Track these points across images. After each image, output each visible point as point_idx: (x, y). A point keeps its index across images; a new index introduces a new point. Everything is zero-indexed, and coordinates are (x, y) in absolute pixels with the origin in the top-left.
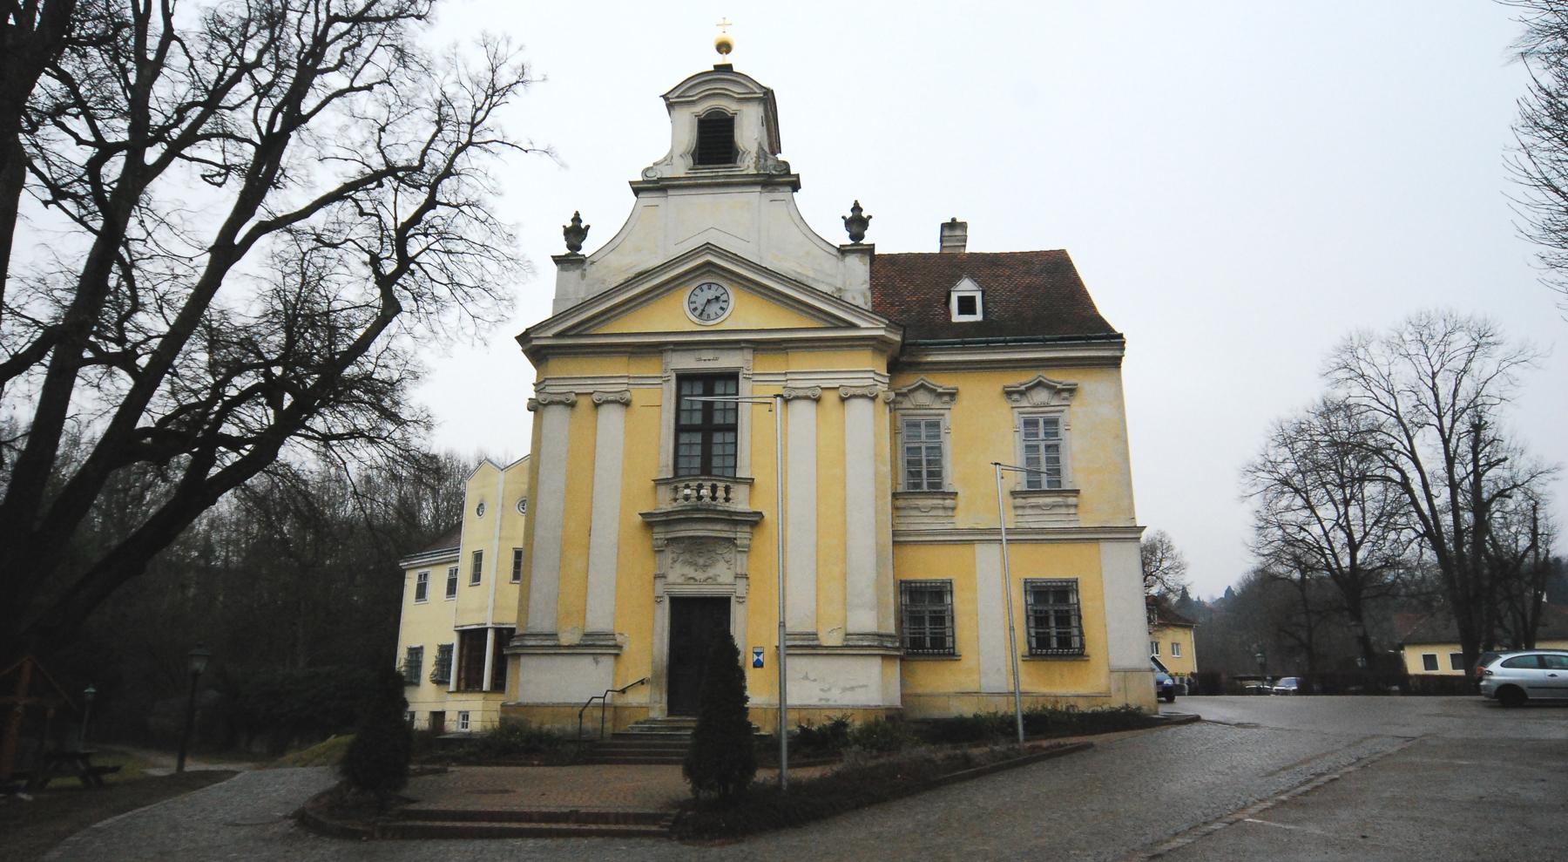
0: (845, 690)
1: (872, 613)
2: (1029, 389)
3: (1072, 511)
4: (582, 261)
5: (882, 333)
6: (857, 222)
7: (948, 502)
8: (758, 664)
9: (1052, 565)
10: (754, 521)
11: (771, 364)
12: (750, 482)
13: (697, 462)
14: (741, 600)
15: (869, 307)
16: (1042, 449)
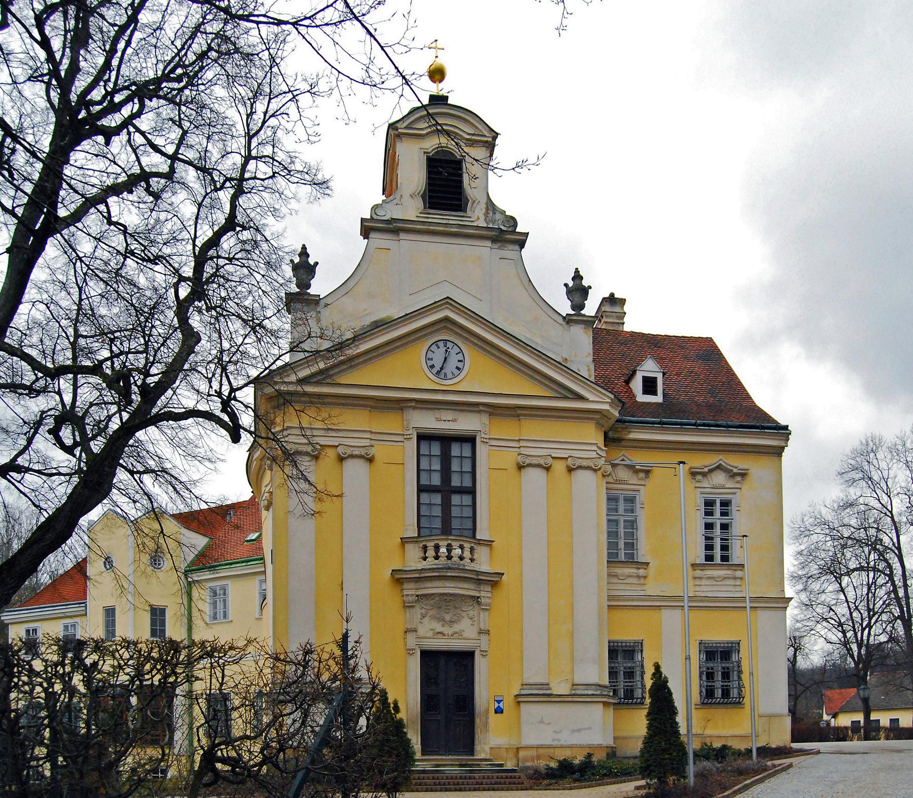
0: (573, 731)
1: (596, 672)
2: (711, 471)
3: (738, 582)
4: (316, 301)
5: (607, 407)
6: (578, 291)
7: (642, 572)
8: (499, 711)
9: (720, 633)
10: (493, 581)
11: (505, 429)
12: (488, 543)
13: (438, 524)
14: (484, 654)
15: (592, 379)
16: (622, 524)
